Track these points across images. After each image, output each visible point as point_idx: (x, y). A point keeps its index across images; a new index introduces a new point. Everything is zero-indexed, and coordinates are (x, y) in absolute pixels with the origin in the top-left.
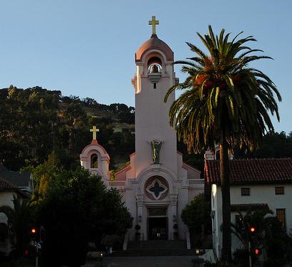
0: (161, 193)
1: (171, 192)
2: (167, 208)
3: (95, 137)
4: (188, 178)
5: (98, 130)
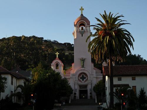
0: (85, 80)
3: (57, 57)
5: (59, 54)
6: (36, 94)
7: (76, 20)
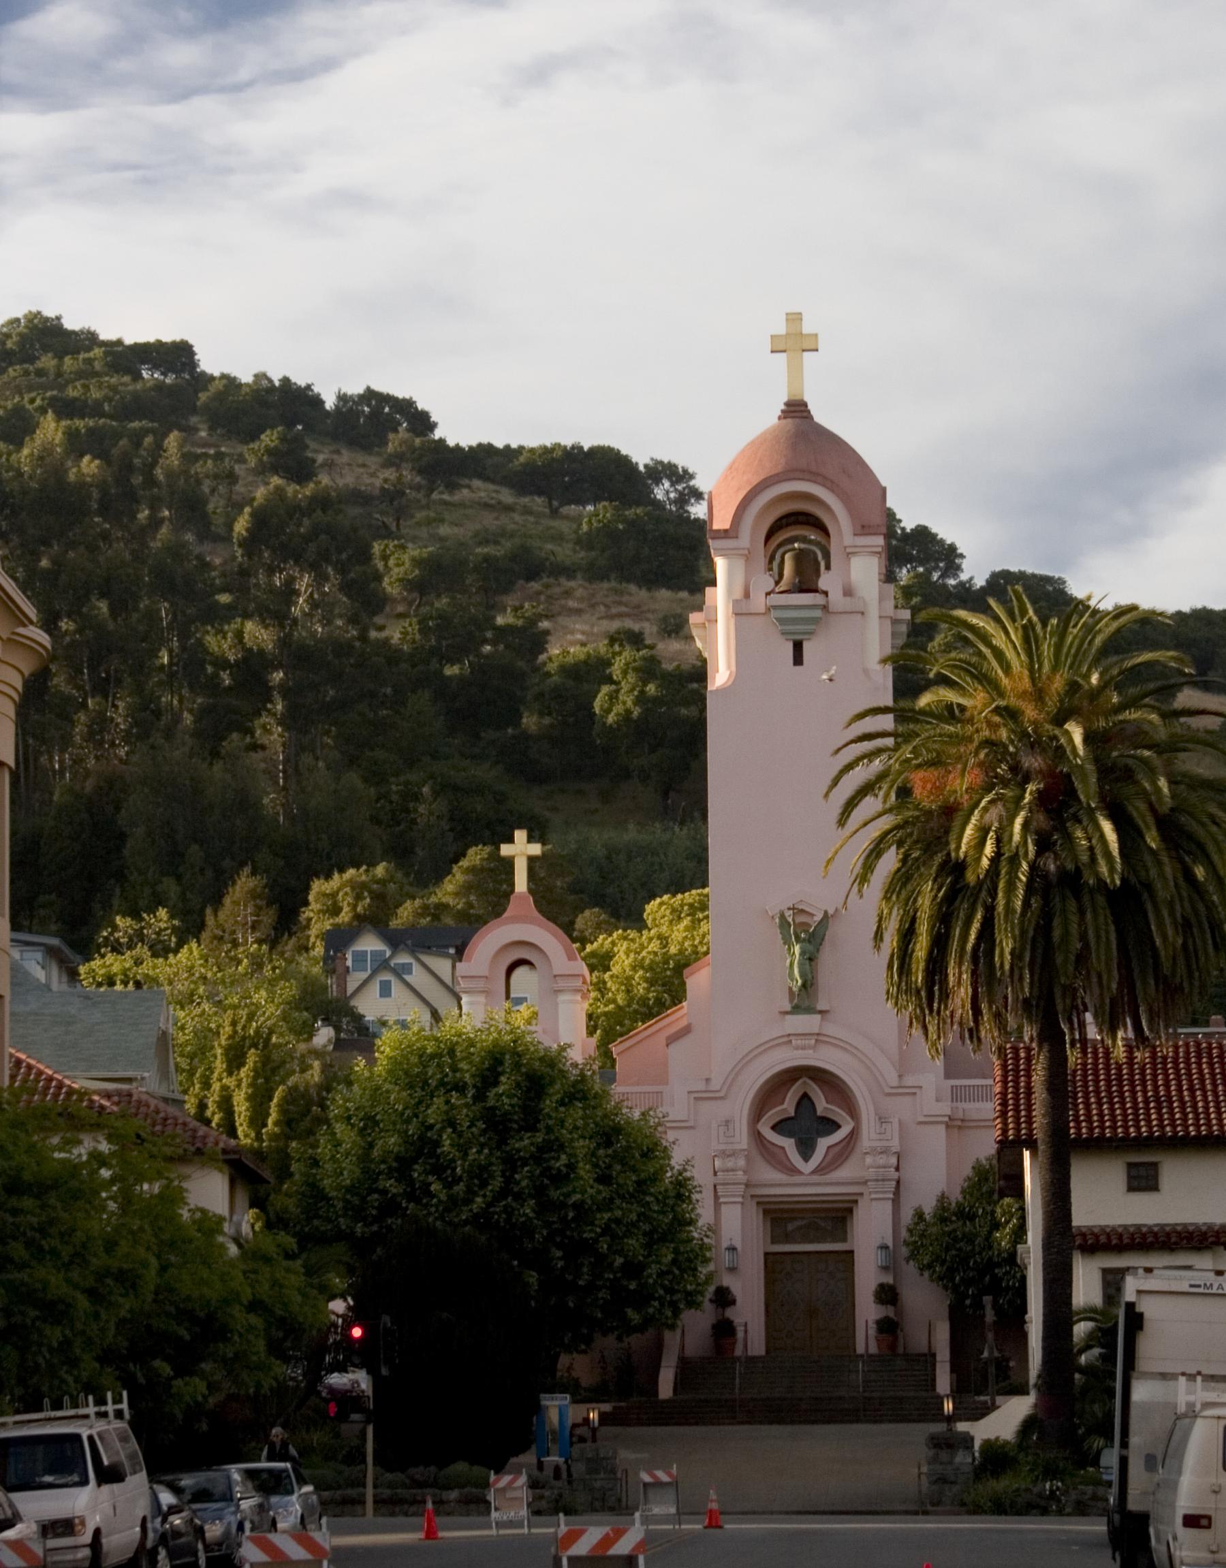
0: (823, 1143)
1: (869, 1136)
2: (850, 1211)
3: (521, 882)
4: (948, 1076)
5: (536, 849)
6: (386, 1319)
7: (755, 445)
